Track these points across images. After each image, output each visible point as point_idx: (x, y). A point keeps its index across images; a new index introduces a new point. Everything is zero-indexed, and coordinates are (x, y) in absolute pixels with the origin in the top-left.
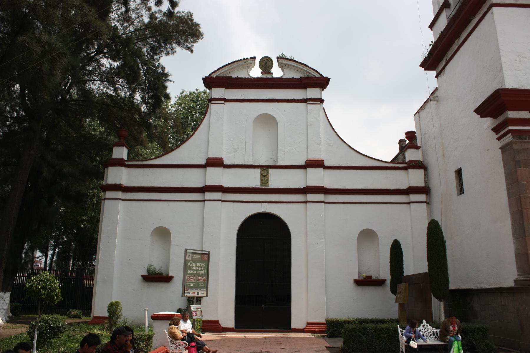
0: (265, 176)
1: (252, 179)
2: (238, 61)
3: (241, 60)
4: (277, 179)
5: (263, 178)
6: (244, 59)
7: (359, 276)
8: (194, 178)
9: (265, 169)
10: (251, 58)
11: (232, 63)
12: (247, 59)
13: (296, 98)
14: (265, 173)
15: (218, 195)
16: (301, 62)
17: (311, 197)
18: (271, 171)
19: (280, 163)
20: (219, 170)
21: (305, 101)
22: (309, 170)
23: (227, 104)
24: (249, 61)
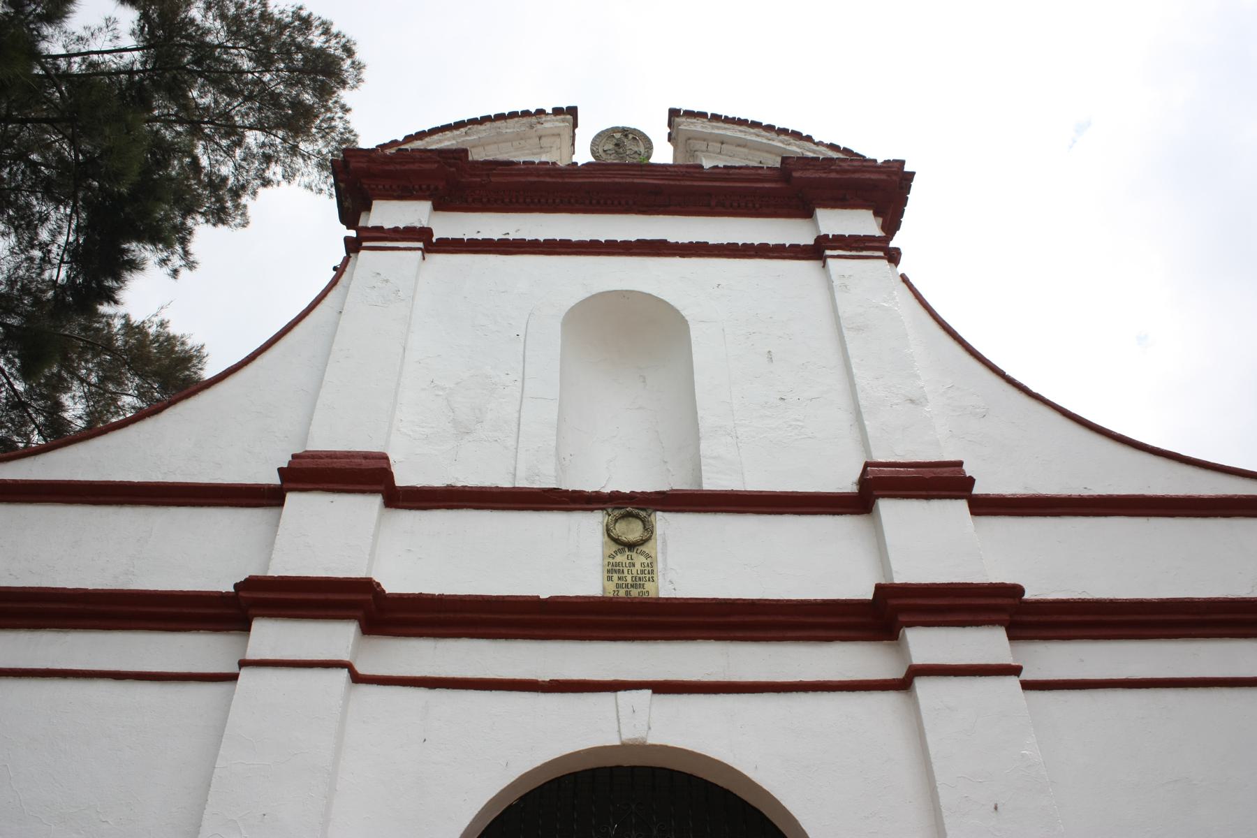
0: (631, 546)
1: (564, 559)
2: (500, 117)
3: (513, 115)
4: (695, 561)
5: (620, 558)
6: (526, 113)
7: (604, 589)
8: (207, 551)
9: (631, 508)
10: (557, 111)
11: (473, 122)
12: (540, 112)
13: (772, 241)
14: (632, 531)
15: (337, 638)
16: (791, 128)
17: (925, 644)
18: (663, 521)
19: (715, 481)
20: (365, 508)
21: (816, 251)
22: (887, 508)
23: (440, 260)
24: (551, 124)
